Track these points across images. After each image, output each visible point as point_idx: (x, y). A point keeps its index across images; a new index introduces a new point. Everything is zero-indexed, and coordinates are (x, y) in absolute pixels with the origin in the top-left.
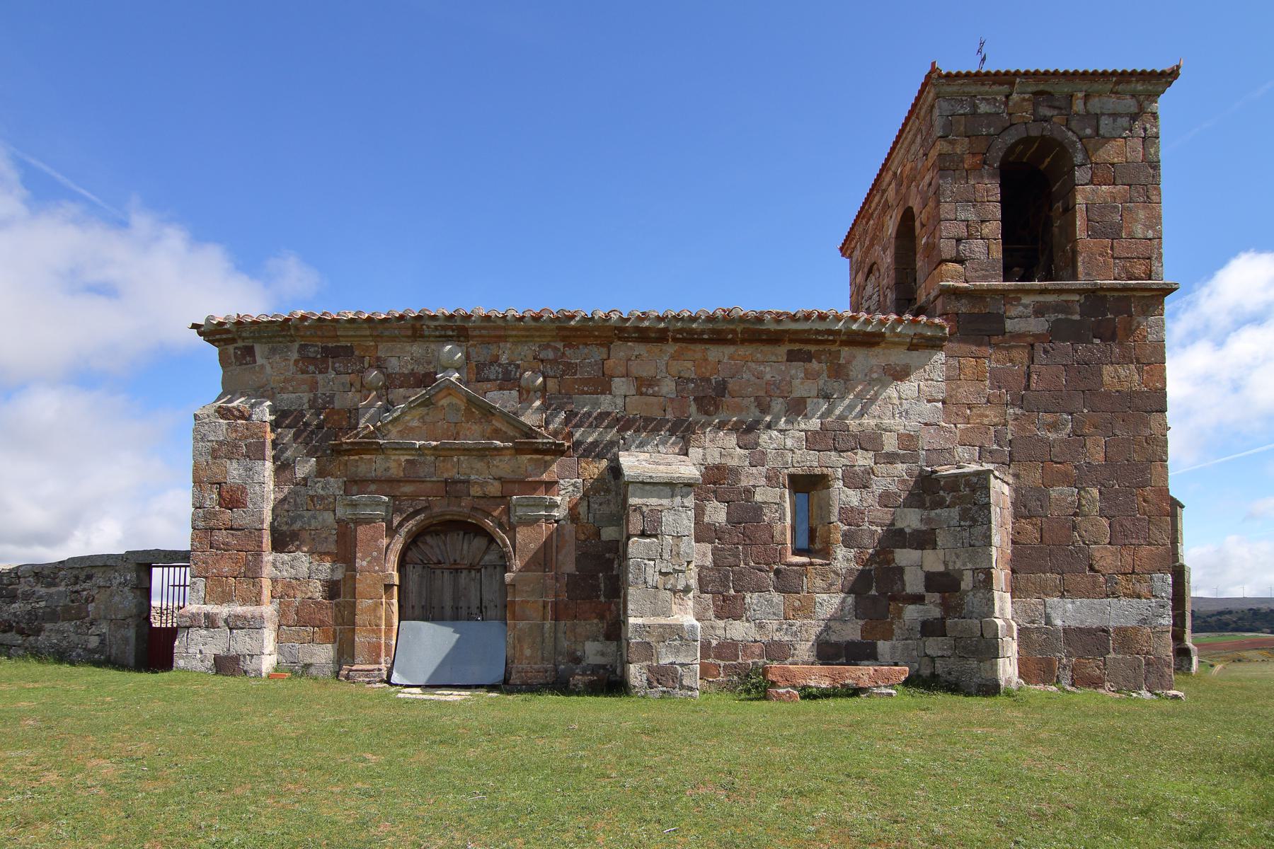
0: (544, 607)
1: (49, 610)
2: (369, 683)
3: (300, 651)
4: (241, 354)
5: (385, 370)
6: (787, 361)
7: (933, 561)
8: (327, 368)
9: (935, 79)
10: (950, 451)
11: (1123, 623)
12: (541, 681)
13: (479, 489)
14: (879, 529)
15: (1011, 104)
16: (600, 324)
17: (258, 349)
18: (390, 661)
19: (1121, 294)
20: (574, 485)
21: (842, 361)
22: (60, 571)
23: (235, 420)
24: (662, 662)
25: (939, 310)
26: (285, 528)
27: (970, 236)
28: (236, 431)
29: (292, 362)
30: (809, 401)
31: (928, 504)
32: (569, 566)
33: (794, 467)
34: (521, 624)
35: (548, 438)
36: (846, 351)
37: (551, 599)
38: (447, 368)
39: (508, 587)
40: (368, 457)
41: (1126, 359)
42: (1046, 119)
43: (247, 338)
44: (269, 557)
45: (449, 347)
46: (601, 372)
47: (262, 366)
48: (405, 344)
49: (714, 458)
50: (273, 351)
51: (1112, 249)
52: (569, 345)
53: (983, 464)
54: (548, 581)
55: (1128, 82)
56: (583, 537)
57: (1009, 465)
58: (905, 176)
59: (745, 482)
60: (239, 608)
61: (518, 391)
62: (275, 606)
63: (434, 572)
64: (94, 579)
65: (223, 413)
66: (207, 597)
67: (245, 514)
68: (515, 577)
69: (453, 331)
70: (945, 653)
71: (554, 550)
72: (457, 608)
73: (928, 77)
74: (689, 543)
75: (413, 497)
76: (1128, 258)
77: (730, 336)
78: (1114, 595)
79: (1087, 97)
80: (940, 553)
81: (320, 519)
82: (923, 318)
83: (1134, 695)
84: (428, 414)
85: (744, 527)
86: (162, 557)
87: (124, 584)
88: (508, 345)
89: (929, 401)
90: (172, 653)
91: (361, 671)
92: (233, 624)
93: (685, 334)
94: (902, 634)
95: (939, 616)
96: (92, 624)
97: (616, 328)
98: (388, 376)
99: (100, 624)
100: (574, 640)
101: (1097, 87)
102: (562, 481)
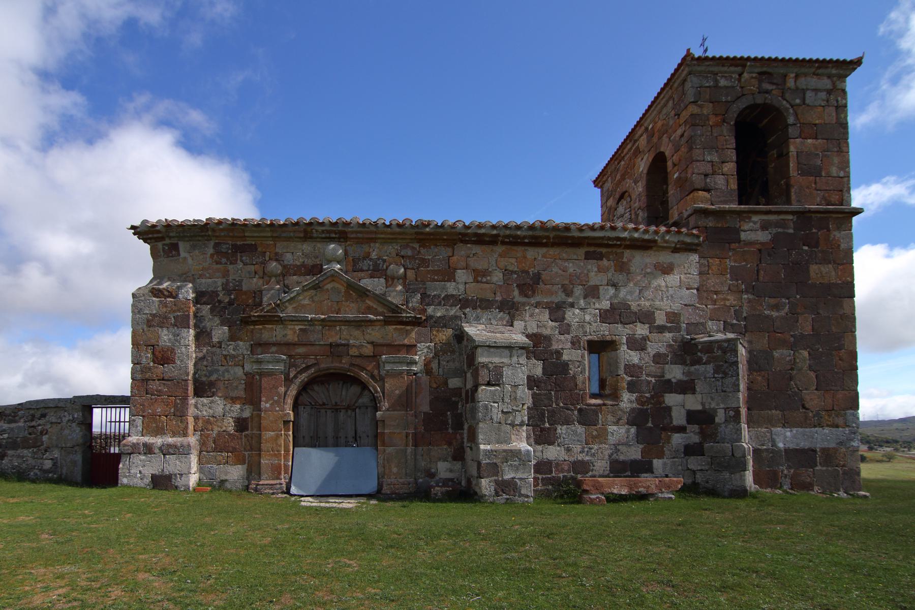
0: (407, 437)
1: (10, 440)
2: (273, 494)
3: (218, 470)
4: (169, 248)
5: (282, 262)
6: (585, 259)
7: (693, 402)
8: (237, 260)
9: (688, 60)
10: (704, 325)
11: (825, 445)
12: (406, 491)
13: (356, 350)
14: (653, 380)
15: (743, 80)
16: (448, 231)
17: (182, 245)
18: (288, 477)
19: (822, 215)
20: (428, 347)
21: (625, 260)
22: (19, 411)
23: (165, 299)
24: (506, 477)
25: (691, 224)
26: (204, 379)
27: (714, 173)
28: (166, 307)
29: (209, 255)
30: (601, 288)
31: (688, 362)
32: (425, 408)
33: (591, 335)
34: (389, 450)
35: (410, 313)
36: (627, 253)
37: (411, 431)
38: (331, 261)
39: (379, 423)
40: (270, 326)
41: (825, 261)
42: (767, 92)
43: (173, 237)
44: (192, 401)
45: (332, 246)
46: (447, 265)
47: (185, 258)
48: (297, 243)
49: (533, 328)
50: (194, 247)
51: (815, 183)
52: (424, 246)
53: (727, 333)
54: (409, 418)
55: (827, 67)
56: (435, 386)
57: (744, 335)
58: (656, 130)
59: (555, 346)
60: (170, 440)
61: (385, 279)
62: (197, 437)
63: (319, 412)
64: (47, 417)
65: (155, 292)
66: (145, 431)
67: (174, 368)
68: (383, 414)
69: (336, 234)
70: (703, 468)
71: (414, 395)
72: (337, 438)
73: (684, 59)
74: (524, 391)
75: (305, 356)
76: (826, 190)
77: (545, 241)
78: (820, 425)
79: (797, 77)
80: (699, 397)
81: (232, 372)
82: (684, 230)
83: (836, 495)
84: (316, 295)
85: (555, 378)
86: (103, 400)
87: (72, 421)
88: (377, 245)
89: (687, 289)
90: (118, 473)
91: (267, 485)
92: (166, 450)
93: (511, 239)
94: (671, 455)
95: (698, 441)
96: (46, 451)
97: (460, 234)
98: (284, 267)
99: (53, 451)
100: (429, 460)
101: (803, 70)
102: (418, 345)
